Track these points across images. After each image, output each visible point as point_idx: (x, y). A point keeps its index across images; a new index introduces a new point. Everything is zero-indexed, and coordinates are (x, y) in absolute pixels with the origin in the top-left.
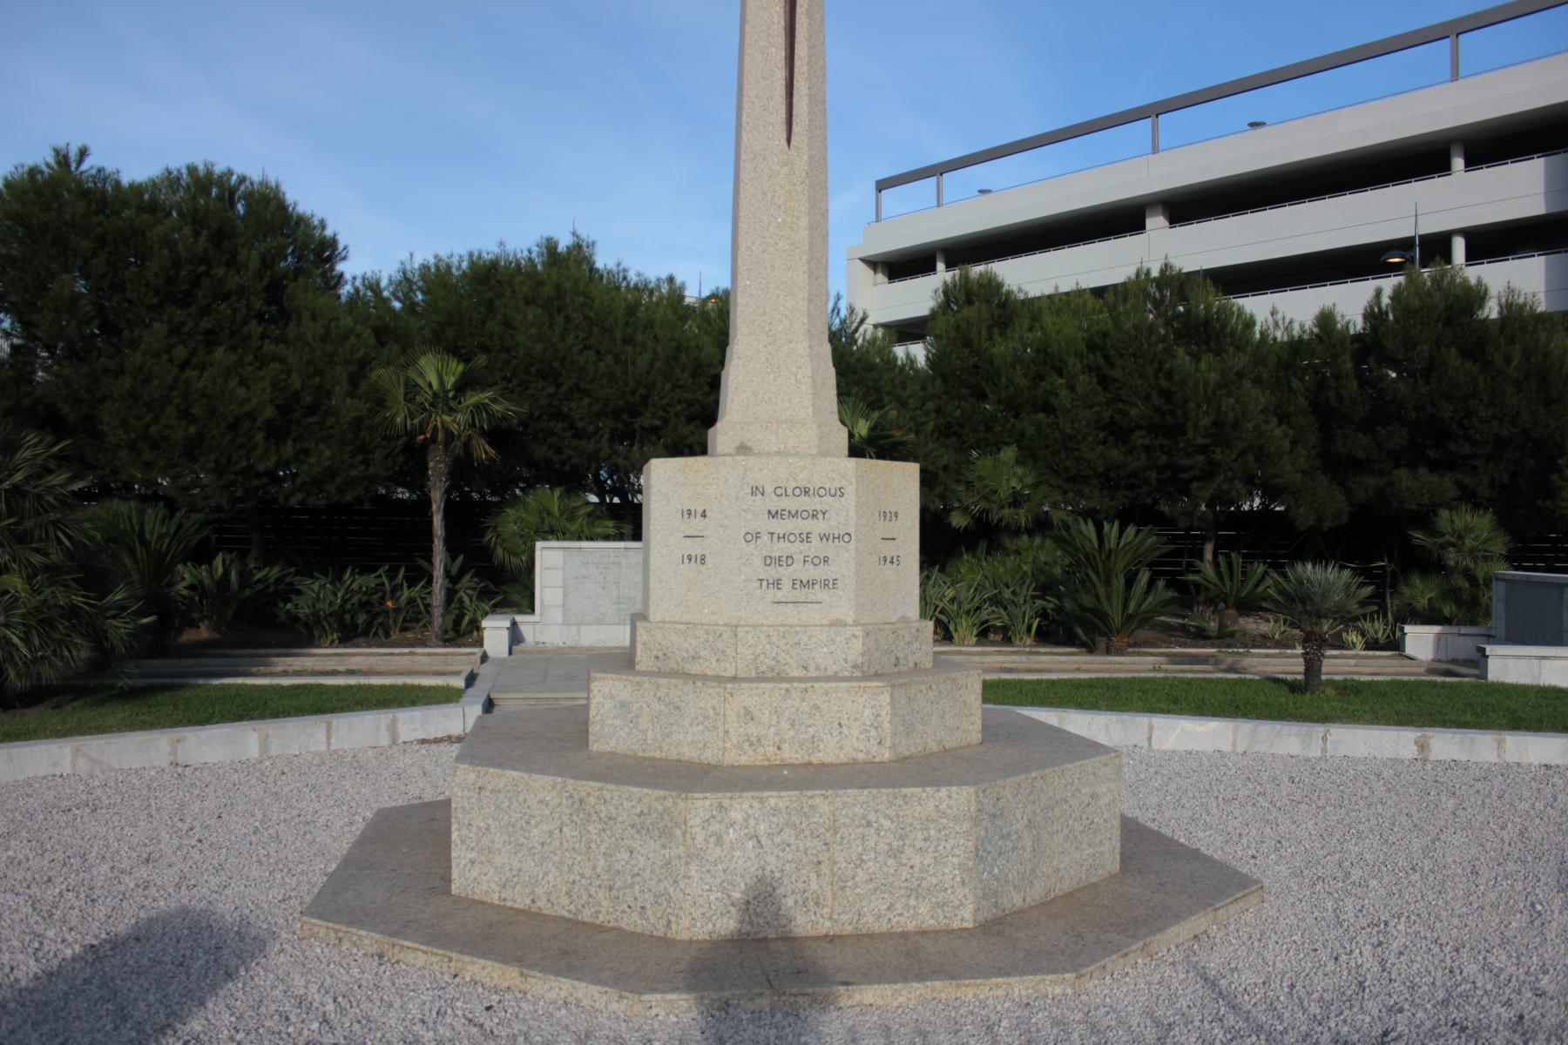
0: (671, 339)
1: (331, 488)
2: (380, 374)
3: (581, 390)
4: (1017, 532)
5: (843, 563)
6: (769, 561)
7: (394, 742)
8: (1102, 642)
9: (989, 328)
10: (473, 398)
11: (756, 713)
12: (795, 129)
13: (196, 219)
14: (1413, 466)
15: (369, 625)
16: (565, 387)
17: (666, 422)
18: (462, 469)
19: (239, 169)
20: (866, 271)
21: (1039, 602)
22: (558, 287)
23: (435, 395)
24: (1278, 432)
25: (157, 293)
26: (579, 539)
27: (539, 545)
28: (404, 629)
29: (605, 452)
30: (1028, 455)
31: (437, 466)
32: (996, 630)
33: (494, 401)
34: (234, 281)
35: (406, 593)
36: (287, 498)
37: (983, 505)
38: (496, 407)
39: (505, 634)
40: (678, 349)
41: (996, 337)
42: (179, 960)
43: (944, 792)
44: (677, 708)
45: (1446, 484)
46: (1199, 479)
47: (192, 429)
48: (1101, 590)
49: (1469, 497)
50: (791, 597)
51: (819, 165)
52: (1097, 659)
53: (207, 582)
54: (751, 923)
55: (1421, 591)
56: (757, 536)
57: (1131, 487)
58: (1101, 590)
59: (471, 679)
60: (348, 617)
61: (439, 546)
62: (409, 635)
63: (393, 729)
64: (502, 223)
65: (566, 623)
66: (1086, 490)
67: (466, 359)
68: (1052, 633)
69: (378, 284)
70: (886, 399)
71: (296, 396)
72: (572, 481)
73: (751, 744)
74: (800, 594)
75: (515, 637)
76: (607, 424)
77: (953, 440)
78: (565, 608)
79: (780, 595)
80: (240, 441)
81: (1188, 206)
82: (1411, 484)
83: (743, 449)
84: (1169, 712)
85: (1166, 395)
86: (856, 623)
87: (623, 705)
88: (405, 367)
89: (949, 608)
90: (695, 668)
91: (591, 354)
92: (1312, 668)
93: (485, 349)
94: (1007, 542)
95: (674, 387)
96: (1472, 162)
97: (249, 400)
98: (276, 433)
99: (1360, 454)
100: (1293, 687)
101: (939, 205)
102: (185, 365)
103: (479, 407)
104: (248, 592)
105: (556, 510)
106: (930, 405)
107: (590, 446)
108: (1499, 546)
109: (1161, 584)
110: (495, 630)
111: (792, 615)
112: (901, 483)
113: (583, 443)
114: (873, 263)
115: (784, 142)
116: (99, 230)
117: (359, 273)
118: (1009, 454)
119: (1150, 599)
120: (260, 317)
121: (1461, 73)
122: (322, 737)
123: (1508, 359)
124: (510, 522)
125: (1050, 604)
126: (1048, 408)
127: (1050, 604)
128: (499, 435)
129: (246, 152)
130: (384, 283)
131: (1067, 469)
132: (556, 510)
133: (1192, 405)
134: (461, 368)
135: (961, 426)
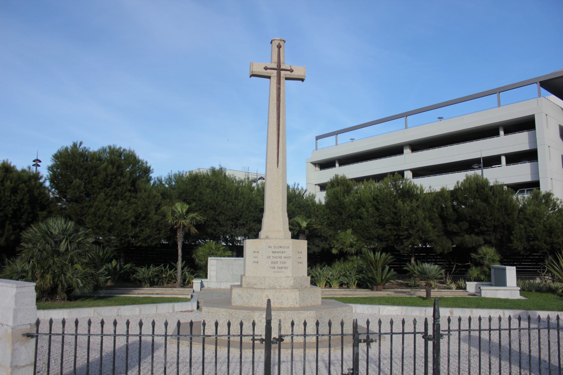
0: (249, 198)
1: (149, 241)
2: (164, 208)
3: (221, 213)
4: (352, 255)
5: (289, 263)
6: (272, 263)
7: (174, 312)
8: (375, 287)
9: (343, 194)
10: (191, 215)
13: (112, 162)
14: (470, 234)
15: (158, 281)
16: (217, 212)
17: (247, 222)
18: (187, 236)
19: (124, 147)
20: (313, 166)
21: (357, 276)
22: (216, 182)
23: (180, 215)
24: (428, 225)
25: (101, 184)
26: (221, 257)
27: (209, 258)
28: (168, 283)
29: (229, 231)
30: (355, 232)
31: (180, 235)
32: (345, 284)
33: (197, 216)
34: (123, 180)
35: (169, 272)
36: (136, 244)
37: (341, 247)
39: (200, 284)
40: (251, 201)
41: (346, 196)
42: (140, 351)
43: (309, 312)
45: (481, 239)
46: (405, 238)
47: (111, 224)
48: (375, 272)
49: (488, 243)
50: (277, 270)
51: (285, 172)
52: (373, 292)
53: (110, 268)
55: (474, 272)
56: (270, 257)
57: (386, 241)
58: (375, 272)
59: (192, 296)
60: (152, 279)
61: (180, 259)
62: (169, 285)
63: (173, 308)
64: (198, 162)
65: (217, 282)
66: (373, 242)
68: (361, 285)
70: (312, 215)
71: (140, 214)
72: (216, 238)
74: (279, 270)
75: (202, 286)
76: (230, 223)
77: (333, 227)
79: (275, 270)
80: (124, 227)
81: (418, 146)
82: (470, 239)
83: (267, 238)
84: (385, 305)
85: (395, 213)
87: (240, 295)
88: (172, 206)
89: (330, 277)
90: (256, 287)
91: (225, 202)
92: (428, 294)
93: (194, 200)
94: (349, 258)
95: (249, 212)
96: (506, 132)
97: (127, 215)
98: (134, 225)
99: (455, 230)
100: (424, 298)
101: (336, 144)
102: (109, 205)
103: (193, 218)
104: (122, 271)
106: (325, 217)
107: (224, 229)
108: (497, 258)
109: (392, 270)
110: (196, 283)
112: (303, 244)
113: (223, 228)
114: (315, 164)
116: (86, 166)
117: (156, 176)
118: (349, 231)
119: (389, 274)
120: (130, 191)
121: (501, 105)
122: (155, 309)
123: (495, 202)
124: (200, 252)
125: (360, 276)
126: (361, 218)
127: (360, 276)
128: (198, 226)
129: (126, 141)
130: (163, 179)
131: (366, 236)
133: (402, 217)
134: (188, 206)
135: (335, 223)
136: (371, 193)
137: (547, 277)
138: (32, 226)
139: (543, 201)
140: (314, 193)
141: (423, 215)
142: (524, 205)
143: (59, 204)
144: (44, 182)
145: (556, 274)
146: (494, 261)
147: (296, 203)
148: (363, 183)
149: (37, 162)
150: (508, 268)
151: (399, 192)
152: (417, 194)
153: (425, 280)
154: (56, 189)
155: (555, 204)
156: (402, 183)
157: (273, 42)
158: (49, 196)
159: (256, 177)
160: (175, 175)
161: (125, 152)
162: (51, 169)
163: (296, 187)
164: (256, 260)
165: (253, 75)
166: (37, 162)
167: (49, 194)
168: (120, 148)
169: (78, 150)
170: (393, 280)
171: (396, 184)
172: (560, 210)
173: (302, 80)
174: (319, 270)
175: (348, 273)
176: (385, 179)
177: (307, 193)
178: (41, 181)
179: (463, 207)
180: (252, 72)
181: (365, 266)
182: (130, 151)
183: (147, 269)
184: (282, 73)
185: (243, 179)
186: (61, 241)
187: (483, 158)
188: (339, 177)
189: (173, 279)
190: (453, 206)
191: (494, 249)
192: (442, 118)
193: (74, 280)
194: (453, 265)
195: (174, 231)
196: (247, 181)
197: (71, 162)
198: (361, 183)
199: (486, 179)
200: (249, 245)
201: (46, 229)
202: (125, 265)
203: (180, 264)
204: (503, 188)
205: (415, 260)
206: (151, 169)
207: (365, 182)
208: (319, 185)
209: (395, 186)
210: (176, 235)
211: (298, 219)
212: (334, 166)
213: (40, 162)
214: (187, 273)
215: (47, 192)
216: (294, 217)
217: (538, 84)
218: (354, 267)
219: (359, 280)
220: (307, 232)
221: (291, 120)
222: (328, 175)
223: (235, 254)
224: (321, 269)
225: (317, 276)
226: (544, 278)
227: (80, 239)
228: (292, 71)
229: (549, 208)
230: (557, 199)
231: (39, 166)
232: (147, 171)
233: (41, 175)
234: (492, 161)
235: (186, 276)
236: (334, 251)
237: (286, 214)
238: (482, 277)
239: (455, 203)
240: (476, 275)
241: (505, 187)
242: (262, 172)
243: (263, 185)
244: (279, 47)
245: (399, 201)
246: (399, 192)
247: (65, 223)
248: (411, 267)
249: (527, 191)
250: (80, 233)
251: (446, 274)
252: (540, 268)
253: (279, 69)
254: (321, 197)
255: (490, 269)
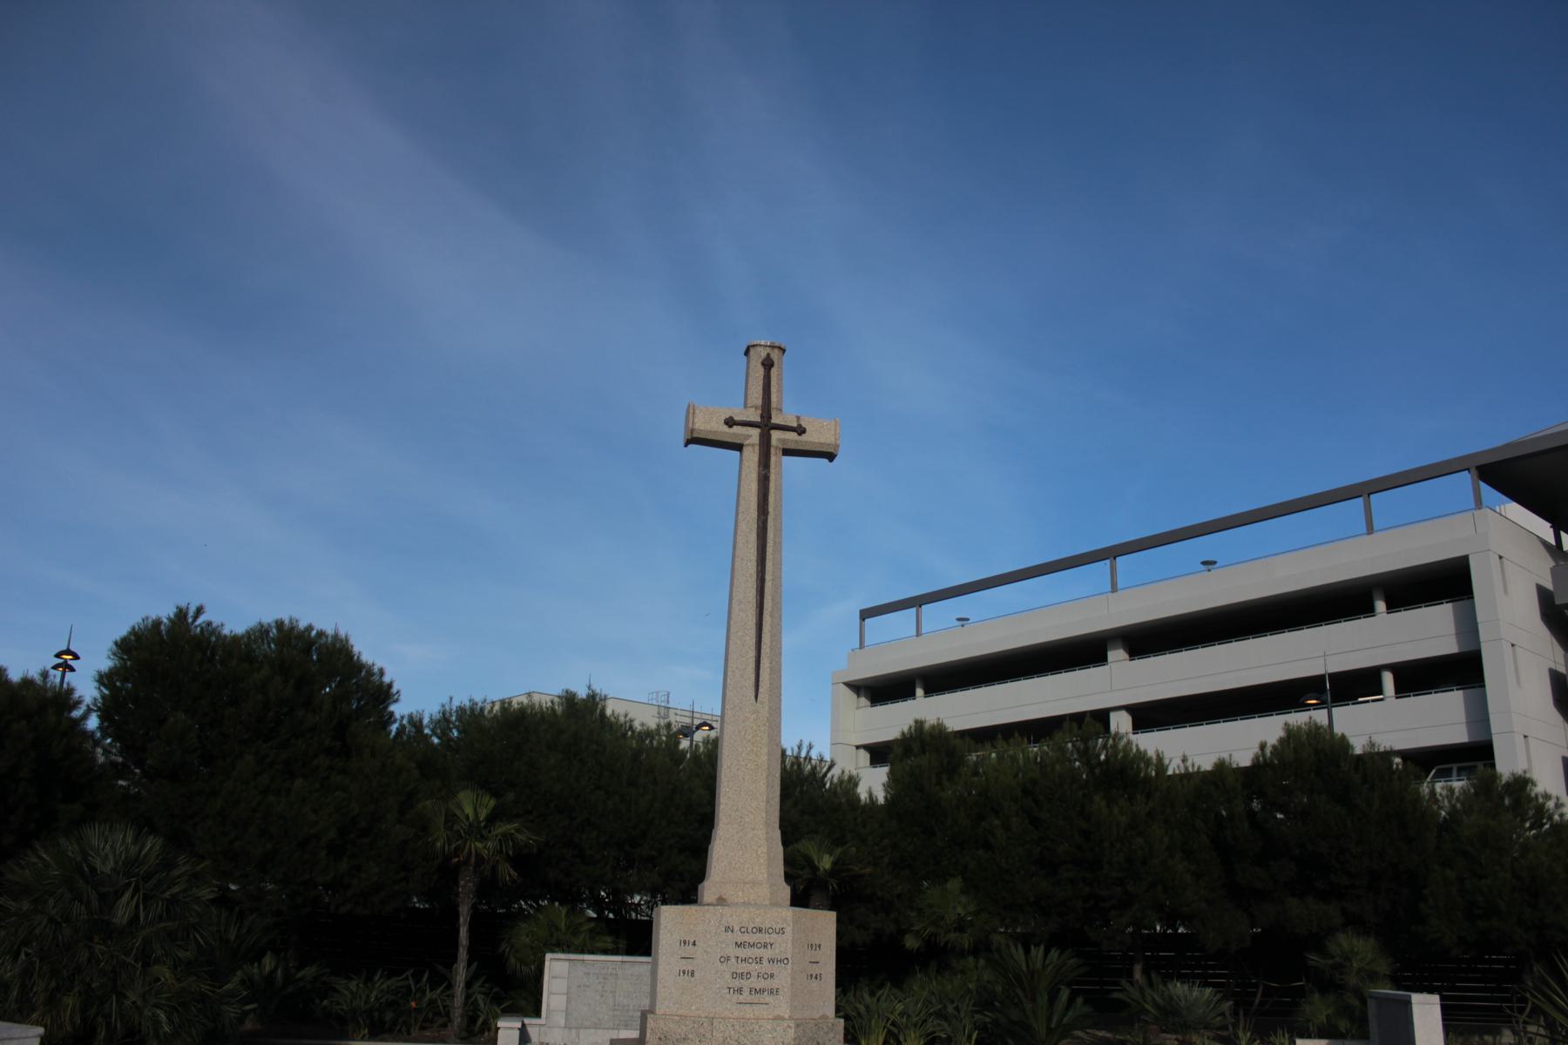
5: (783, 977)
6: (735, 975)
10: (502, 828)
18: (487, 887)
19: (319, 625)
20: (849, 694)
21: (977, 1016)
23: (471, 825)
26: (582, 952)
27: (548, 956)
28: (423, 1028)
31: (466, 885)
33: (518, 831)
35: (429, 995)
37: (930, 930)
38: (520, 837)
48: (1028, 1006)
51: (776, 712)
55: (1319, 1008)
56: (728, 959)
58: (1028, 1006)
60: (376, 1014)
61: (463, 954)
62: (428, 1033)
64: (531, 677)
65: (568, 1027)
67: (496, 794)
69: (421, 721)
72: (570, 899)
74: (756, 998)
78: (568, 1013)
81: (1147, 640)
83: (721, 901)
86: (791, 1018)
89: (898, 1020)
101: (918, 634)
103: (506, 836)
105: (563, 926)
106: (886, 841)
108: (1383, 967)
109: (1080, 1000)
111: (749, 1012)
112: (824, 924)
114: (857, 687)
117: (406, 713)
118: (954, 885)
124: (523, 935)
125: (987, 1018)
127: (987, 1018)
128: (520, 860)
129: (320, 613)
130: (426, 721)
132: (563, 926)
134: (492, 803)
136: (1016, 776)
137: (1532, 1028)
138: (37, 845)
139: (1507, 802)
140: (854, 773)
141: (1166, 840)
142: (1453, 812)
143: (121, 783)
144: (85, 717)
145: (1560, 1018)
146: (1373, 977)
147: (805, 798)
148: (994, 746)
149: (66, 659)
150: (1417, 999)
151: (1097, 771)
152: (1148, 778)
153: (1175, 1032)
154: (116, 738)
155: (1541, 811)
156: (1105, 746)
157: (752, 351)
158: (94, 759)
159: (688, 721)
160: (461, 710)
161: (323, 640)
162: (104, 679)
163: (803, 754)
165: (693, 440)
166: (66, 659)
167: (94, 752)
168: (310, 628)
169: (188, 629)
170: (1082, 1029)
171: (1087, 749)
172: (1559, 828)
173: (831, 457)
174: (866, 996)
175: (950, 1009)
176: (1058, 736)
177: (836, 772)
178: (76, 714)
179: (1279, 816)
180: (692, 431)
181: (999, 989)
182: (336, 636)
183: (365, 983)
184: (776, 436)
185: (653, 726)
186: (118, 895)
187: (1333, 676)
188: (927, 726)
189: (439, 1014)
190: (1251, 814)
191: (1372, 940)
192: (1214, 563)
193: (147, 1012)
194: (1256, 986)
195: (448, 873)
196: (663, 732)
197: (167, 661)
198: (988, 746)
199: (1343, 736)
200: (670, 921)
201: (79, 859)
202: (299, 969)
203: (461, 973)
204: (1391, 763)
205: (1146, 972)
206: (394, 690)
207: (1000, 743)
208: (867, 747)
209: (1086, 755)
210: (456, 883)
211: (808, 847)
212: (912, 695)
213: (76, 657)
214: (480, 998)
215: (88, 745)
216: (797, 841)
217: (1473, 470)
218: (969, 991)
219: (982, 1028)
220: (833, 884)
221: (795, 563)
222: (893, 720)
223: (622, 944)
224: (872, 994)
225: (859, 1014)
226: (1526, 1033)
227: (176, 889)
228: (801, 431)
229: (1523, 821)
230: (1547, 797)
231: (72, 669)
232: (383, 694)
233: (76, 695)
234: (1356, 685)
235: (475, 1003)
236: (911, 942)
237: (778, 833)
238: (1343, 1025)
239: (1256, 805)
240: (1323, 1018)
241: (1398, 760)
242: (710, 706)
243: (713, 746)
244: (768, 364)
245: (1097, 798)
246: (1097, 771)
247: (136, 840)
248: (1135, 994)
249: (1460, 770)
250: (176, 873)
251: (1235, 1013)
252: (1509, 1000)
253: (766, 425)
254: (873, 783)
255: (1364, 1001)
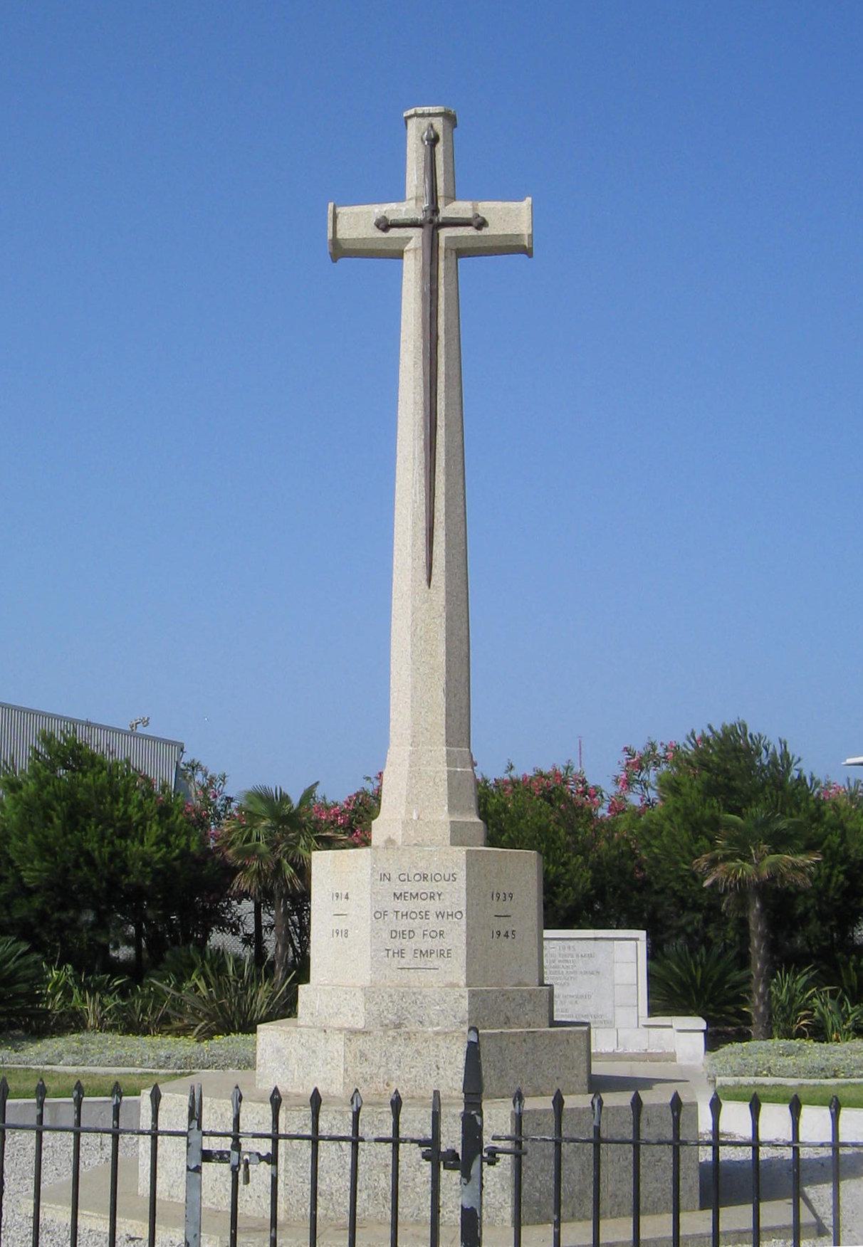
6: (394, 934)
11: (370, 1056)
12: (434, 571)
44: (314, 1052)
54: (334, 1210)
56: (385, 913)
73: (366, 1081)
74: (420, 962)
115: (424, 582)
164: (504, 925)
228: (482, 224)
